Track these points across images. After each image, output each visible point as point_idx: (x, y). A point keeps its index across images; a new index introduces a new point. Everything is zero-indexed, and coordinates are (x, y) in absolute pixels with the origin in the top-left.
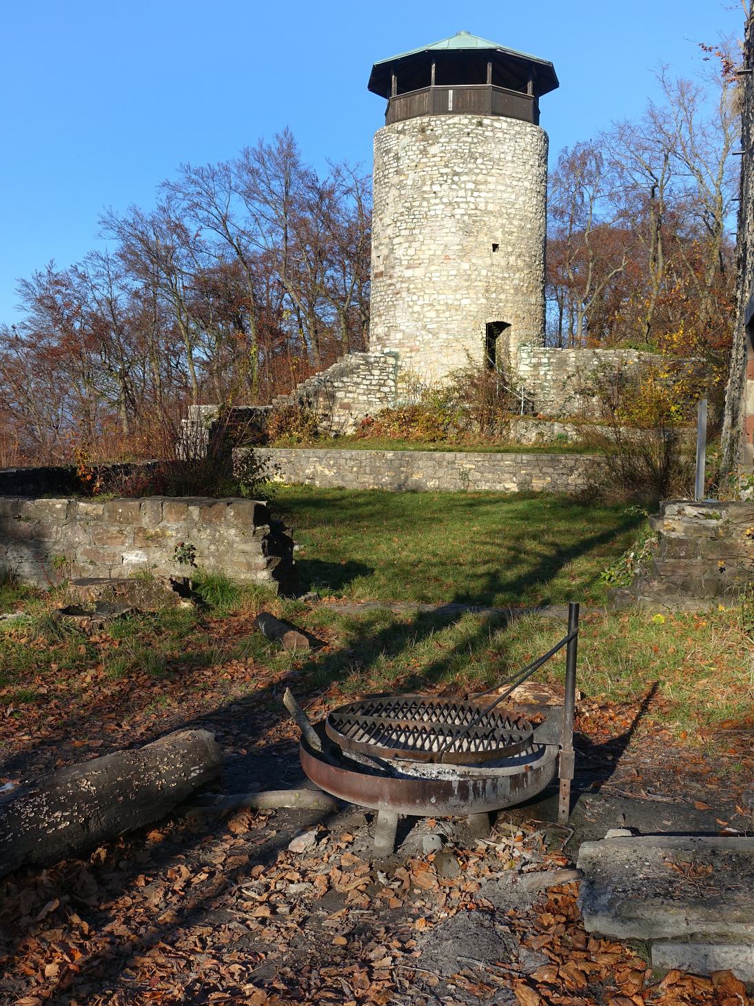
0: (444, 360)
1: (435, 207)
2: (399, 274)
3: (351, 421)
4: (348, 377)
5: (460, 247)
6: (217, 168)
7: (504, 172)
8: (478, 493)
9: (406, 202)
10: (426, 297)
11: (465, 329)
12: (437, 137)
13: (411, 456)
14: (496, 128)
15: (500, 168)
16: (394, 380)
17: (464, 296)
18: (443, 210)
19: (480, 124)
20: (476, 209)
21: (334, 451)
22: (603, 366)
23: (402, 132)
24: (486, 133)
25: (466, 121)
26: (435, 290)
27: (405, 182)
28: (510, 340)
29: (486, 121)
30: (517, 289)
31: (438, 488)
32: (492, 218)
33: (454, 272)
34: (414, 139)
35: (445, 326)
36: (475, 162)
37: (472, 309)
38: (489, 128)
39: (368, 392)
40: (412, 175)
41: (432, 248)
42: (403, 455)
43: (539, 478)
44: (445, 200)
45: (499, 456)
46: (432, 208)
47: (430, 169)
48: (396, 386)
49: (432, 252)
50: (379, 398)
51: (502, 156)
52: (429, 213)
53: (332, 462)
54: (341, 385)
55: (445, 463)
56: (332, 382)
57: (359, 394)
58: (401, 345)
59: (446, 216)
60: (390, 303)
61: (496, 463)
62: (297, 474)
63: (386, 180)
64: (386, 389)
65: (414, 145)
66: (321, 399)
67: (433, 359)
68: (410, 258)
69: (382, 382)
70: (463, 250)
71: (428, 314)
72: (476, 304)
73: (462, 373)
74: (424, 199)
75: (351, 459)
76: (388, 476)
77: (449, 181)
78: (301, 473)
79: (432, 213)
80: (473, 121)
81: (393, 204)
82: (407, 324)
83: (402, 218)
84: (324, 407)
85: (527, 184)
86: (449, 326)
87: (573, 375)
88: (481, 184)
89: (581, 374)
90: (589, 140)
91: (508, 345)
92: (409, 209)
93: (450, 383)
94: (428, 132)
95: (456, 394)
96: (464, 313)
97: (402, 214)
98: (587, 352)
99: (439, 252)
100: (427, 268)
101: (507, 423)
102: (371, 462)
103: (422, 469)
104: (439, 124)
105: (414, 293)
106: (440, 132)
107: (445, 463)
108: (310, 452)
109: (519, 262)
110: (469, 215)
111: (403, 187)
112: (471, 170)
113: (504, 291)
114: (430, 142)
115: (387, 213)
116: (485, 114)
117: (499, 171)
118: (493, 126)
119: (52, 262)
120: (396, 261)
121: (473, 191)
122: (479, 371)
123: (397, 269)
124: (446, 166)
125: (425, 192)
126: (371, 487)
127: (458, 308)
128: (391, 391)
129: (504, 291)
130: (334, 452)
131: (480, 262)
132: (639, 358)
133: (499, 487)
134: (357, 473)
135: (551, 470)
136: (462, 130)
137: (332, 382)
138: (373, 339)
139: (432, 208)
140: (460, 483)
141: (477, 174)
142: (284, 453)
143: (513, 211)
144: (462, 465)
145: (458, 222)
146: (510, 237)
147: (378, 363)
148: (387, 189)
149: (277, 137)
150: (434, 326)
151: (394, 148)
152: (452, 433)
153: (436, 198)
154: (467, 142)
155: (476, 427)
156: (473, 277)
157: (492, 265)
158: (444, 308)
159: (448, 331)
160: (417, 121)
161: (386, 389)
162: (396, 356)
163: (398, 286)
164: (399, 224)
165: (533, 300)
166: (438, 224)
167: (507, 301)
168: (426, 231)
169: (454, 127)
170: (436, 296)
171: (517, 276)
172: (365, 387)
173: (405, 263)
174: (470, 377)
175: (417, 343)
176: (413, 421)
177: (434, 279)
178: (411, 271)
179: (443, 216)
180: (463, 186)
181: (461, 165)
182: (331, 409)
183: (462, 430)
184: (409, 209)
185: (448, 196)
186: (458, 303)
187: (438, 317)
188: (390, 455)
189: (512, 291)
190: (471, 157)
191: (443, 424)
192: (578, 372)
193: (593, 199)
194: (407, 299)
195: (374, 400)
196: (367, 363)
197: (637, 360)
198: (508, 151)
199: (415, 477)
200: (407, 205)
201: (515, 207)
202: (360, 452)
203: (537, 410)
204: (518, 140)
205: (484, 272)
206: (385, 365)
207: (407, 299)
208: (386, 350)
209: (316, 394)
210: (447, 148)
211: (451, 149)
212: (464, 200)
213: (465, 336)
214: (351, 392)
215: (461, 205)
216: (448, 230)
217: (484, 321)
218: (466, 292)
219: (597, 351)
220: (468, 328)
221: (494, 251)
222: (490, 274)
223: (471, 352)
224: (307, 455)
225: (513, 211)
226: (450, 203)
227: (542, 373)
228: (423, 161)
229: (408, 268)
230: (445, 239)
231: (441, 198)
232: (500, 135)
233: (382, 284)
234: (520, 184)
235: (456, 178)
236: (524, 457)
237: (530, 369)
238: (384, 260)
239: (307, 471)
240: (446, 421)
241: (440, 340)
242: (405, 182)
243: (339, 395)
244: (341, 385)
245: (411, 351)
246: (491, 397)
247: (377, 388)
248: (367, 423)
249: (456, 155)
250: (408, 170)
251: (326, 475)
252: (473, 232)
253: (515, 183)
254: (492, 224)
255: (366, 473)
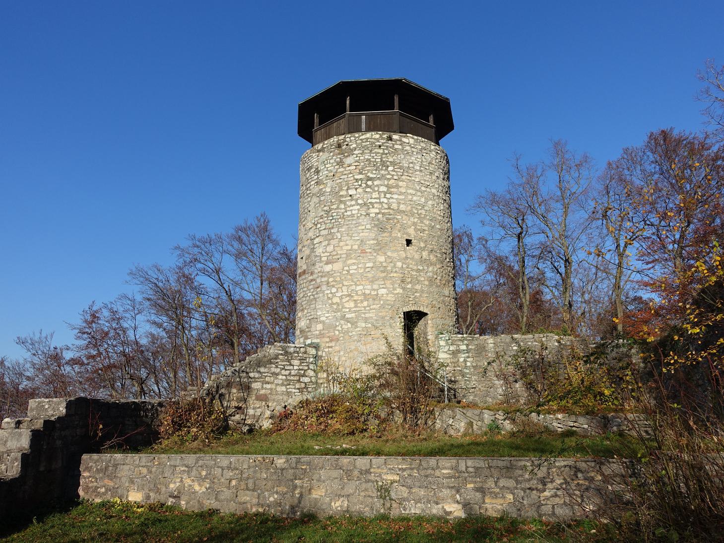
0: (363, 348)
1: (351, 208)
2: (319, 269)
3: (268, 413)
4: (265, 367)
5: (375, 242)
6: (214, 237)
7: (413, 179)
8: (404, 519)
9: (325, 206)
10: (344, 288)
11: (383, 318)
12: (352, 150)
13: (309, 463)
14: (405, 142)
15: (410, 175)
16: (314, 371)
17: (381, 286)
18: (358, 210)
19: (390, 139)
20: (389, 208)
21: (208, 457)
22: (523, 351)
23: (322, 150)
24: (396, 146)
26: (353, 281)
27: (324, 190)
28: (428, 328)
29: (395, 137)
30: (431, 281)
31: (348, 511)
32: (405, 217)
33: (370, 265)
34: (332, 154)
35: (363, 315)
36: (386, 169)
37: (389, 298)
38: (398, 142)
39: (287, 383)
40: (330, 183)
41: (349, 244)
42: (298, 462)
43: (495, 496)
44: (360, 201)
45: (432, 461)
46: (348, 209)
47: (346, 176)
48: (316, 377)
49: (349, 247)
50: (299, 389)
51: (411, 165)
52: (345, 214)
53: (204, 473)
54: (257, 375)
55: (356, 473)
56: (247, 373)
57: (277, 385)
58: (321, 335)
59: (361, 215)
60: (312, 297)
61: (429, 471)
62: (158, 491)
63: (308, 192)
64: (306, 380)
65: (332, 159)
66: (234, 391)
67: (353, 347)
68: (329, 254)
69: (302, 372)
70: (378, 244)
71: (347, 305)
72: (393, 294)
73: (381, 361)
74: (341, 202)
75: (229, 468)
76: (277, 493)
77: (364, 185)
78: (164, 489)
79: (349, 213)
80: (384, 136)
81: (314, 211)
82: (327, 315)
83: (321, 220)
84: (237, 399)
85: (434, 191)
86: (367, 315)
87: (494, 361)
88: (393, 187)
89: (501, 360)
90: (462, 226)
91: (425, 334)
92: (328, 212)
93: (369, 370)
94: (344, 147)
95: (377, 383)
96: (382, 302)
97: (321, 217)
98: (505, 338)
99: (356, 247)
100: (345, 262)
101: (432, 412)
102: (255, 472)
103: (324, 482)
104: (353, 140)
105: (333, 286)
106: (354, 146)
107: (356, 473)
108: (176, 459)
109: (432, 257)
110: (383, 214)
111: (323, 195)
112: (383, 175)
113: (419, 282)
114: (346, 154)
115: (309, 219)
116: (395, 132)
117: (409, 178)
118: (401, 141)
119: (93, 302)
120: (317, 259)
121: (385, 193)
122: (399, 359)
123: (318, 265)
124: (361, 173)
126: (254, 510)
127: (376, 298)
128: (311, 382)
129: (419, 282)
130: (207, 459)
131: (395, 255)
132: (559, 342)
133: (435, 510)
134: (237, 488)
135: (511, 483)
136: (374, 143)
137: (247, 373)
138: (298, 333)
139: (348, 209)
140: (378, 504)
141: (389, 179)
142: (144, 460)
143: (423, 212)
144: (380, 476)
145: (373, 220)
146: (421, 234)
147: (298, 353)
148: (309, 199)
150: (353, 315)
151: (315, 165)
152: (373, 424)
153: (352, 200)
154: (379, 153)
155: (398, 417)
156: (389, 268)
157: (407, 258)
158: (362, 298)
159: (366, 320)
160: (334, 139)
161: (306, 380)
162: (316, 347)
163: (318, 281)
164: (319, 226)
165: (446, 292)
166: (354, 222)
167: (422, 291)
168: (343, 230)
169: (367, 141)
170: (353, 287)
171: (431, 269)
172: (284, 377)
173: (324, 259)
174: (390, 364)
175: (337, 333)
176: (333, 412)
177: (351, 272)
178: (330, 266)
179: (359, 215)
180: (376, 189)
181: (374, 172)
182: (245, 400)
183: (384, 421)
184: (328, 212)
185: (363, 198)
186: (376, 293)
187: (356, 307)
188: (280, 461)
189: (427, 283)
190: (383, 165)
191: (363, 414)
192: (498, 357)
193: (468, 261)
194: (326, 292)
195: (294, 390)
196: (286, 353)
197: (557, 344)
198: (416, 162)
199: (315, 494)
201: (426, 208)
202: (241, 457)
203: (460, 395)
204: (424, 154)
205: (399, 264)
206: (305, 355)
207: (326, 292)
208: (308, 342)
209: (229, 385)
211: (365, 159)
212: (378, 201)
213: (384, 325)
214: (268, 383)
215: (376, 205)
216: (364, 227)
217: (401, 310)
218: (383, 283)
219: (515, 336)
220: (386, 316)
221: (408, 245)
222: (405, 266)
223: (390, 339)
224: (172, 463)
225: (423, 212)
226: (365, 204)
227: (462, 360)
228: (339, 170)
229: (327, 263)
230: (361, 234)
231: (357, 200)
232: (408, 148)
233: (305, 281)
234: (428, 190)
235: (370, 183)
236: (470, 463)
237: (449, 356)
238: (306, 260)
239: (172, 486)
240: (366, 411)
241: (358, 329)
242: (324, 190)
243: (255, 386)
244: (257, 375)
245: (331, 341)
246: (413, 384)
247: (297, 378)
248: (286, 415)
249: (370, 164)
250: (326, 180)
251: (195, 492)
252: (387, 229)
253: (423, 189)
254: (405, 222)
255: (248, 489)
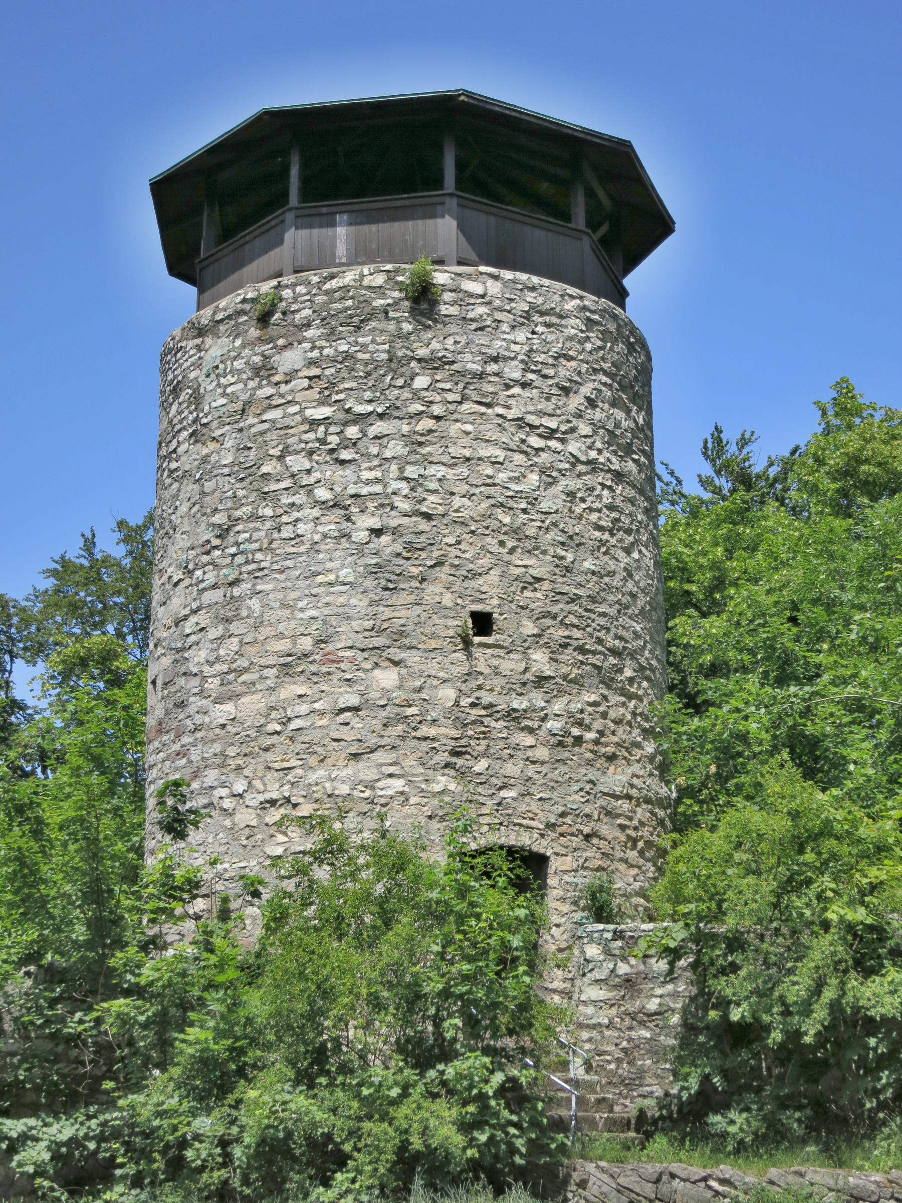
14: (471, 295)
25: (380, 280)
44: (322, 493)
68: (225, 668)
114: (281, 342)
125: (266, 477)
149: (83, 535)
200: (220, 519)
210: (326, 351)
216: (332, 577)
235: (352, 432)
253: (535, 441)
